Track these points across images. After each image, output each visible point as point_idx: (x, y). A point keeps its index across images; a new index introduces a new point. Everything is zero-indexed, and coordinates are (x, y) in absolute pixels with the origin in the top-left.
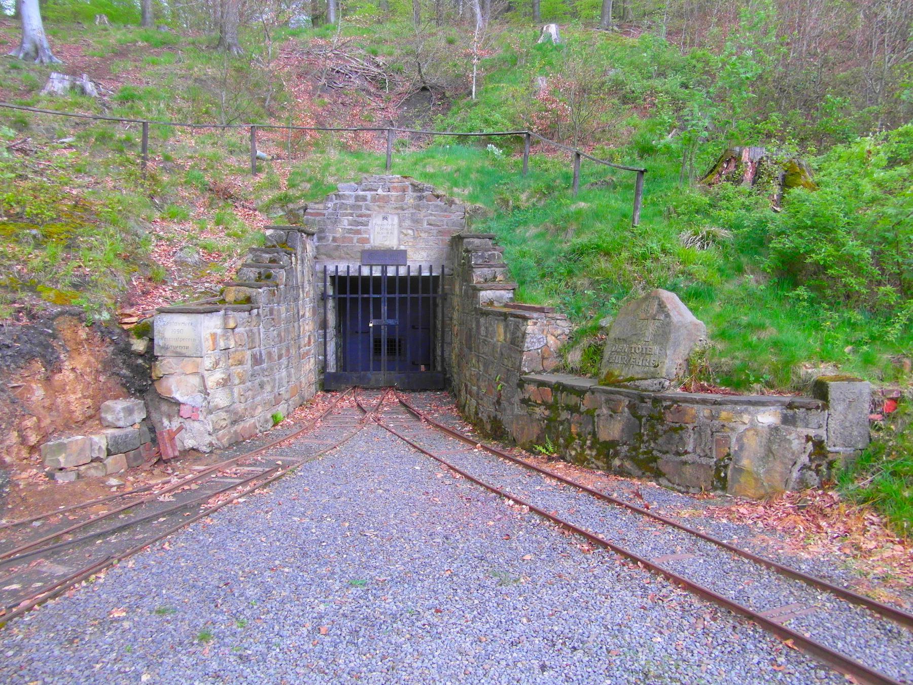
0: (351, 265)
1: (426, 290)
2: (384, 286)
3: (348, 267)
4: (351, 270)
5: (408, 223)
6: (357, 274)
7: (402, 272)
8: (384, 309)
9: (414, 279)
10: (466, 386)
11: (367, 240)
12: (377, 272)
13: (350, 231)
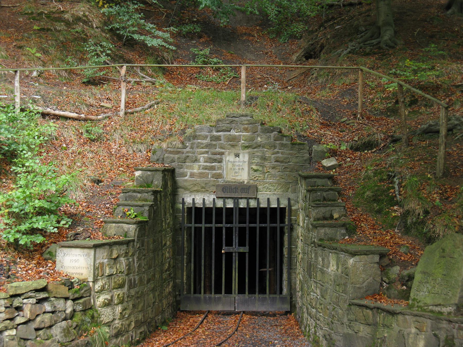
0: (206, 198)
1: (273, 220)
2: (236, 217)
3: (204, 199)
4: (207, 202)
5: (257, 160)
6: (212, 206)
7: (253, 204)
8: (236, 239)
9: (263, 210)
10: (307, 309)
11: (219, 176)
12: (230, 204)
13: (205, 168)
